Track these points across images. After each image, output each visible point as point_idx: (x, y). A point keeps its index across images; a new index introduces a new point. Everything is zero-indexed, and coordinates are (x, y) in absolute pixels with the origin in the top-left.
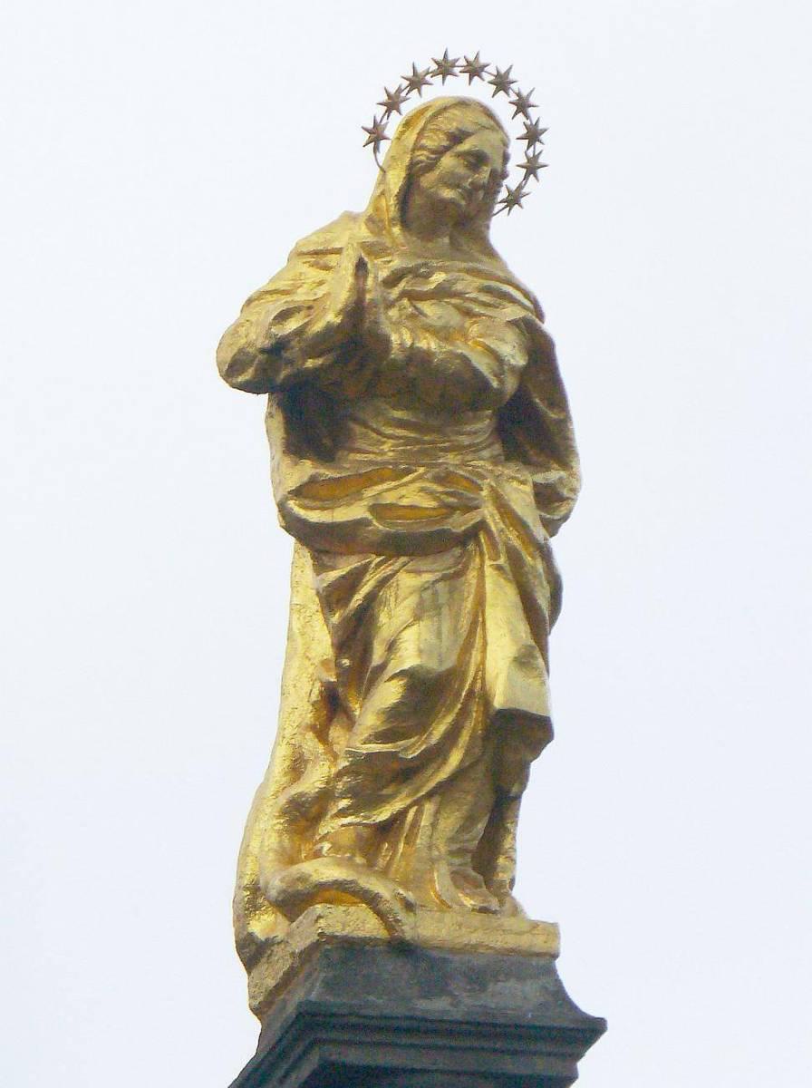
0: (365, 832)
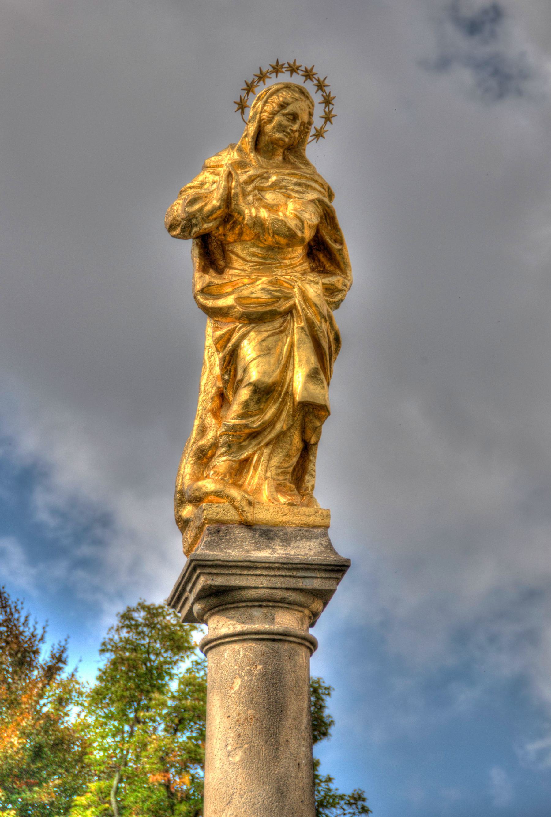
0: (235, 465)
